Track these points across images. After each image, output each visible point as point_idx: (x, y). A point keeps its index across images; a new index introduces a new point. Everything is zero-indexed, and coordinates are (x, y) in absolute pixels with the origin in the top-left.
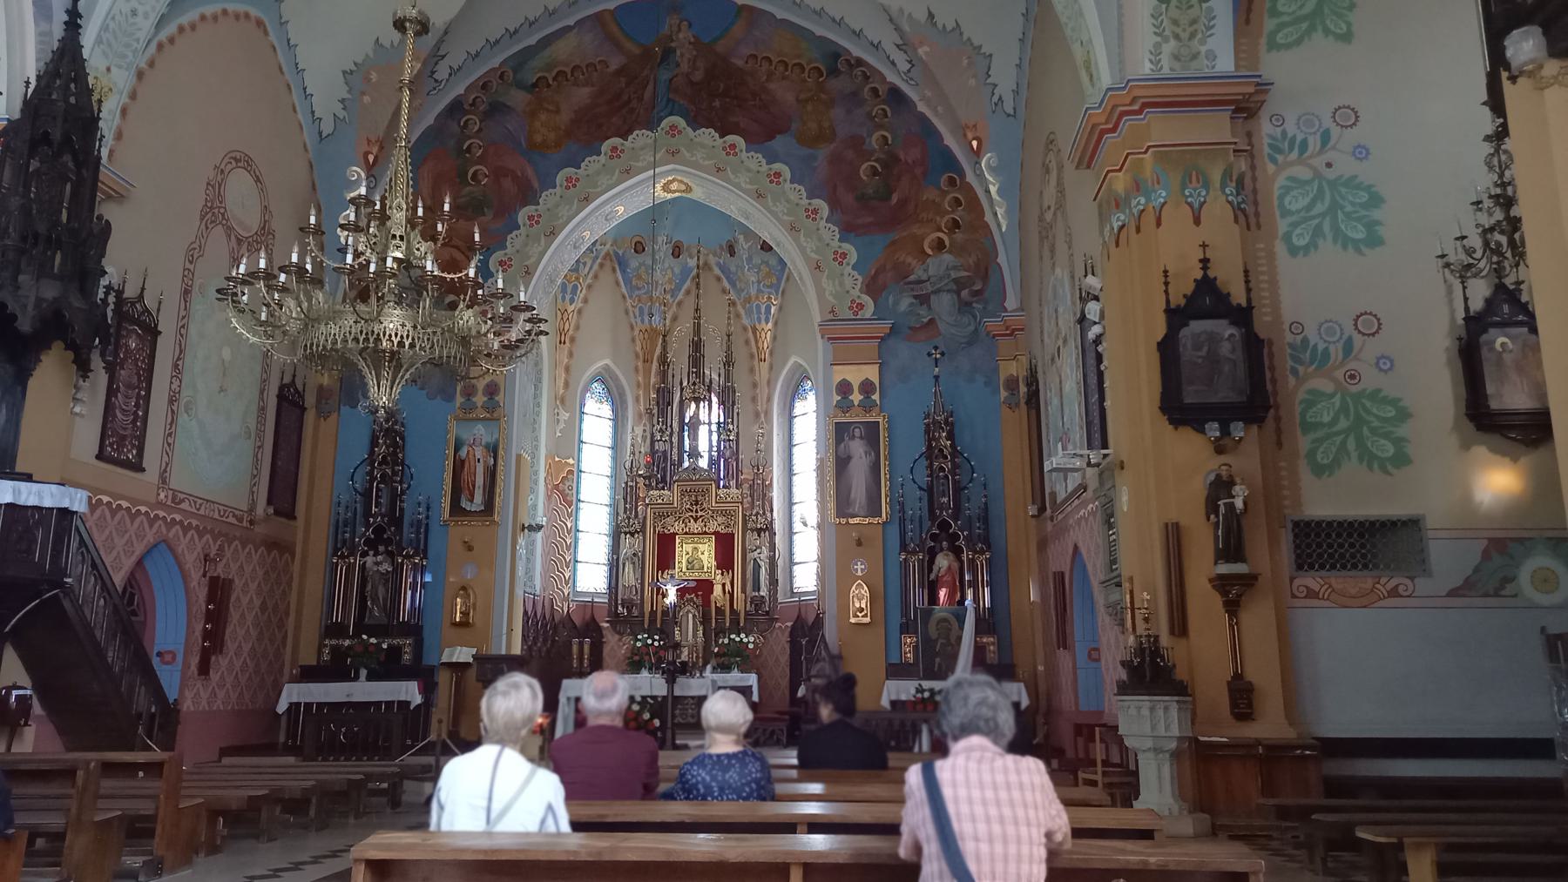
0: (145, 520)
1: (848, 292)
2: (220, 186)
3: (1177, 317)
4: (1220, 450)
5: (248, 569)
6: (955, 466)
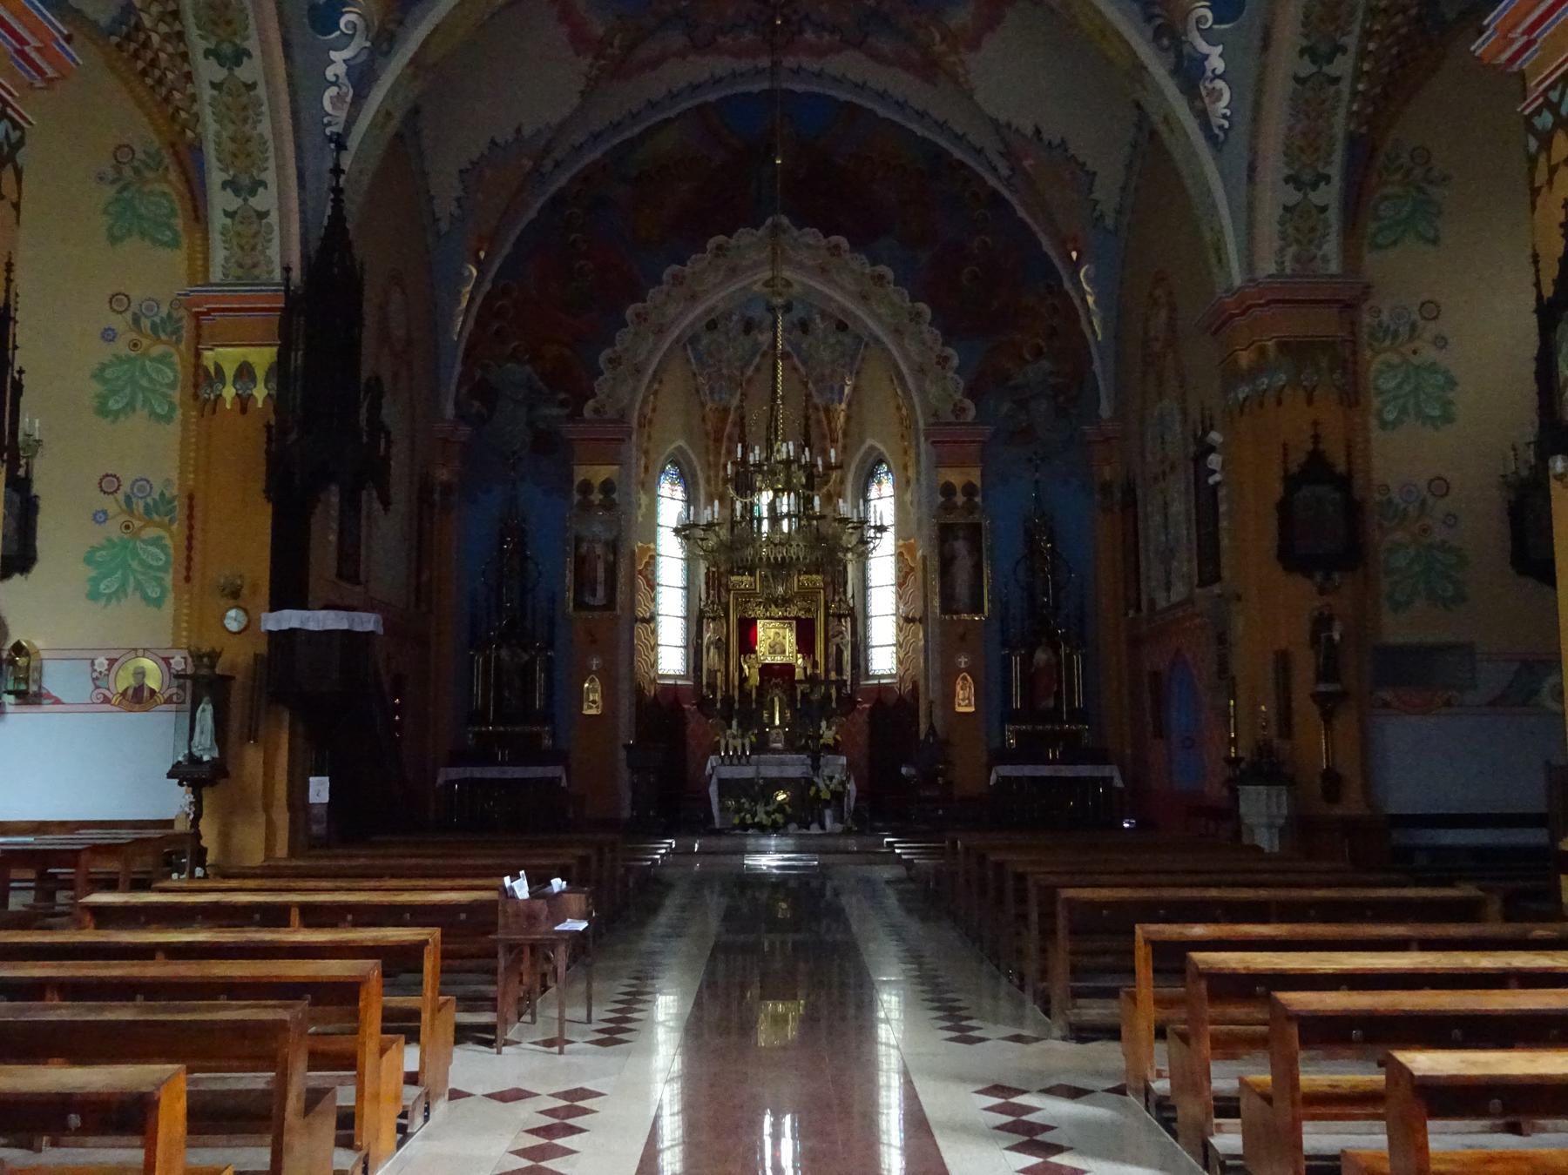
3: (1292, 482)
4: (1322, 591)
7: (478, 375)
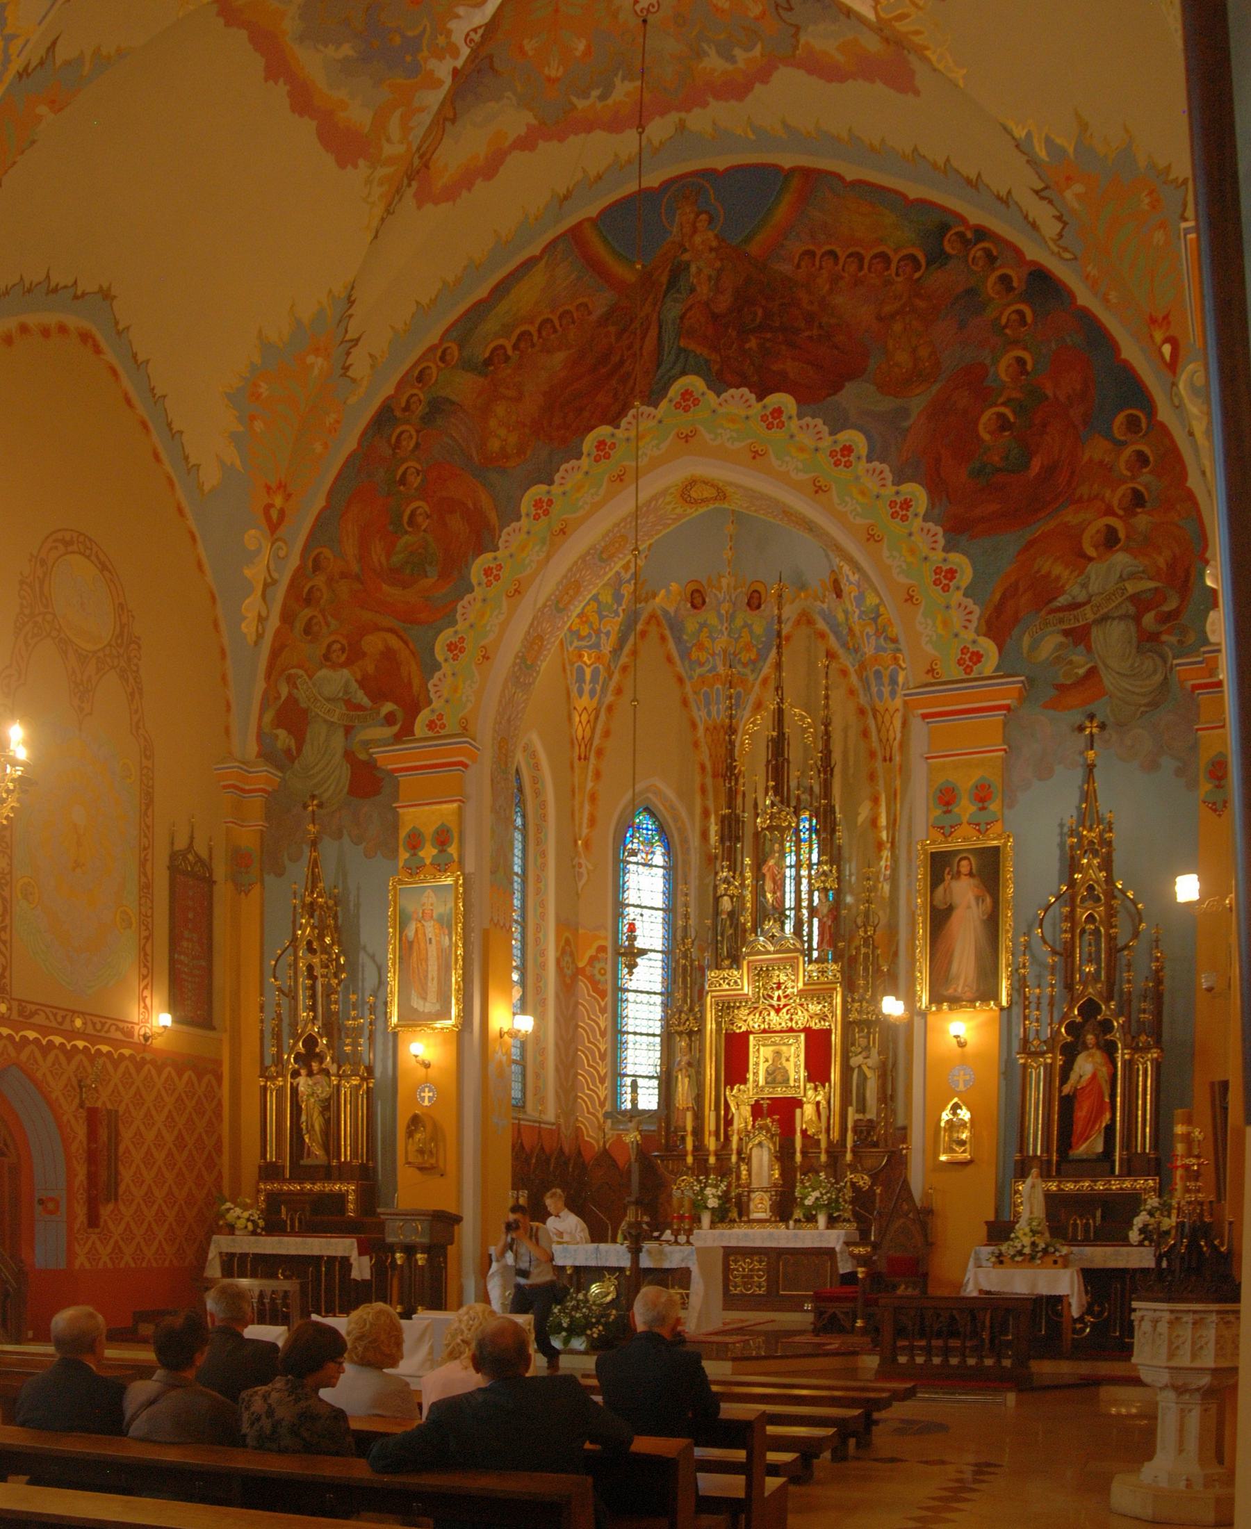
1: (956, 635)
6: (1111, 913)
7: (284, 690)
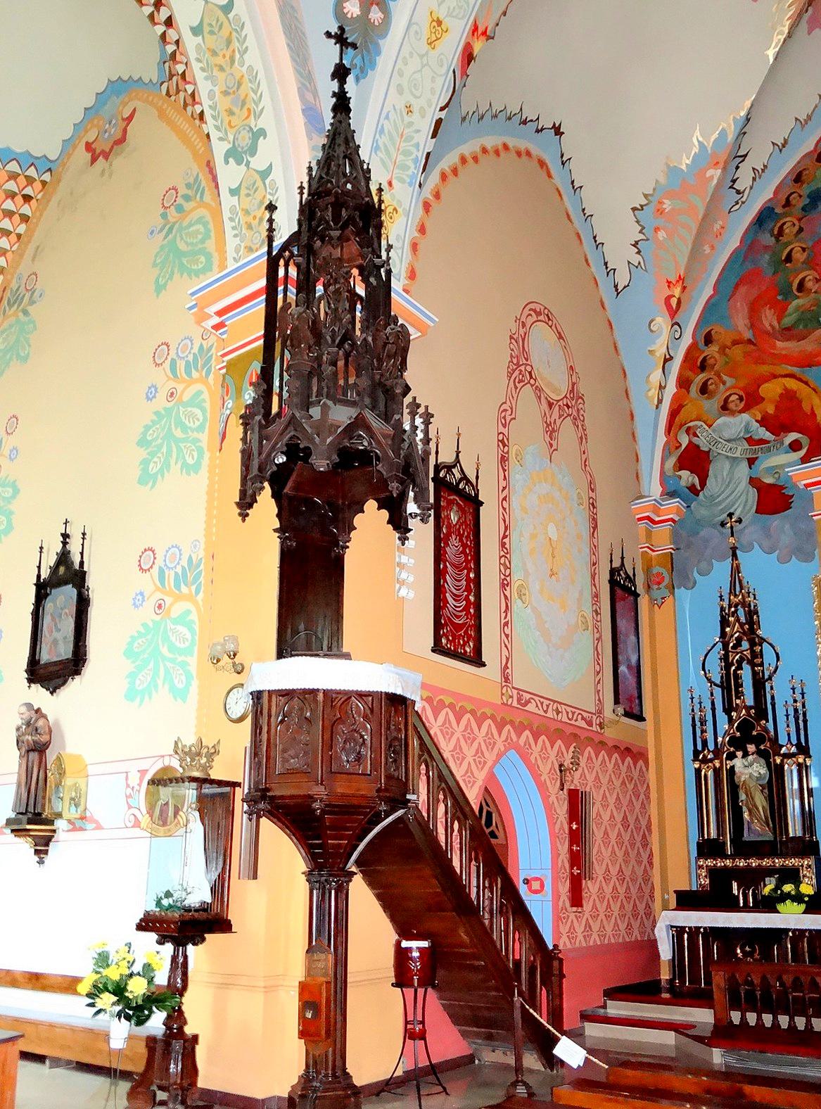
0: (472, 718)
2: (523, 340)
5: (604, 780)
7: (684, 440)
